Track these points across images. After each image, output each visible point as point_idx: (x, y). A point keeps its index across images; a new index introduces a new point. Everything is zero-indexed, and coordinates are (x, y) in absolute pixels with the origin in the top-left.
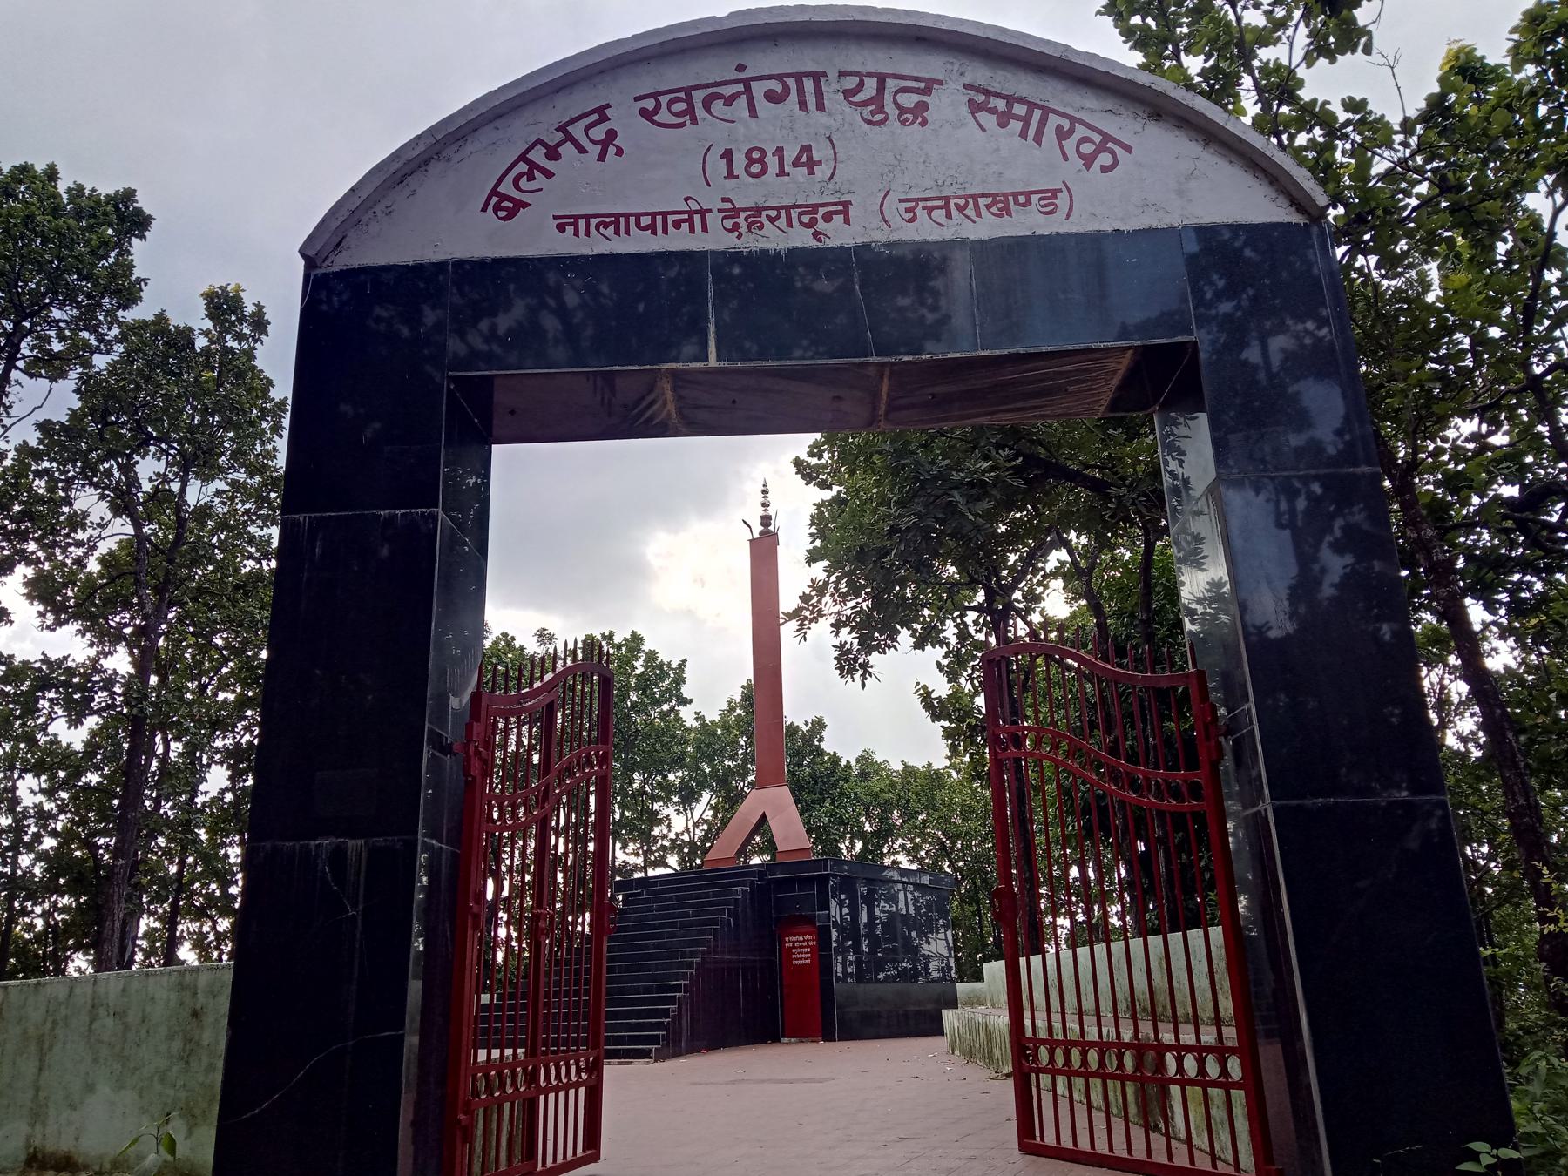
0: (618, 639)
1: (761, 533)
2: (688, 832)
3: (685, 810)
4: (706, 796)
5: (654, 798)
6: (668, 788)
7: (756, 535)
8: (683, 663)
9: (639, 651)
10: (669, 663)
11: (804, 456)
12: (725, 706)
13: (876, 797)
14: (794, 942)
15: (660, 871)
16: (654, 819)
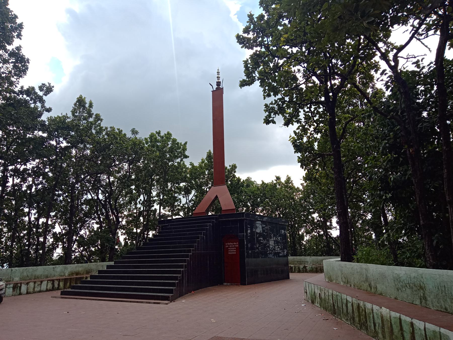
0: (162, 134)
1: (216, 88)
2: (187, 204)
3: (186, 196)
4: (193, 192)
5: (175, 192)
6: (180, 189)
7: (215, 89)
8: (186, 143)
9: (170, 139)
10: (181, 143)
11: (241, 33)
12: (201, 161)
14: (229, 245)
16: (176, 200)
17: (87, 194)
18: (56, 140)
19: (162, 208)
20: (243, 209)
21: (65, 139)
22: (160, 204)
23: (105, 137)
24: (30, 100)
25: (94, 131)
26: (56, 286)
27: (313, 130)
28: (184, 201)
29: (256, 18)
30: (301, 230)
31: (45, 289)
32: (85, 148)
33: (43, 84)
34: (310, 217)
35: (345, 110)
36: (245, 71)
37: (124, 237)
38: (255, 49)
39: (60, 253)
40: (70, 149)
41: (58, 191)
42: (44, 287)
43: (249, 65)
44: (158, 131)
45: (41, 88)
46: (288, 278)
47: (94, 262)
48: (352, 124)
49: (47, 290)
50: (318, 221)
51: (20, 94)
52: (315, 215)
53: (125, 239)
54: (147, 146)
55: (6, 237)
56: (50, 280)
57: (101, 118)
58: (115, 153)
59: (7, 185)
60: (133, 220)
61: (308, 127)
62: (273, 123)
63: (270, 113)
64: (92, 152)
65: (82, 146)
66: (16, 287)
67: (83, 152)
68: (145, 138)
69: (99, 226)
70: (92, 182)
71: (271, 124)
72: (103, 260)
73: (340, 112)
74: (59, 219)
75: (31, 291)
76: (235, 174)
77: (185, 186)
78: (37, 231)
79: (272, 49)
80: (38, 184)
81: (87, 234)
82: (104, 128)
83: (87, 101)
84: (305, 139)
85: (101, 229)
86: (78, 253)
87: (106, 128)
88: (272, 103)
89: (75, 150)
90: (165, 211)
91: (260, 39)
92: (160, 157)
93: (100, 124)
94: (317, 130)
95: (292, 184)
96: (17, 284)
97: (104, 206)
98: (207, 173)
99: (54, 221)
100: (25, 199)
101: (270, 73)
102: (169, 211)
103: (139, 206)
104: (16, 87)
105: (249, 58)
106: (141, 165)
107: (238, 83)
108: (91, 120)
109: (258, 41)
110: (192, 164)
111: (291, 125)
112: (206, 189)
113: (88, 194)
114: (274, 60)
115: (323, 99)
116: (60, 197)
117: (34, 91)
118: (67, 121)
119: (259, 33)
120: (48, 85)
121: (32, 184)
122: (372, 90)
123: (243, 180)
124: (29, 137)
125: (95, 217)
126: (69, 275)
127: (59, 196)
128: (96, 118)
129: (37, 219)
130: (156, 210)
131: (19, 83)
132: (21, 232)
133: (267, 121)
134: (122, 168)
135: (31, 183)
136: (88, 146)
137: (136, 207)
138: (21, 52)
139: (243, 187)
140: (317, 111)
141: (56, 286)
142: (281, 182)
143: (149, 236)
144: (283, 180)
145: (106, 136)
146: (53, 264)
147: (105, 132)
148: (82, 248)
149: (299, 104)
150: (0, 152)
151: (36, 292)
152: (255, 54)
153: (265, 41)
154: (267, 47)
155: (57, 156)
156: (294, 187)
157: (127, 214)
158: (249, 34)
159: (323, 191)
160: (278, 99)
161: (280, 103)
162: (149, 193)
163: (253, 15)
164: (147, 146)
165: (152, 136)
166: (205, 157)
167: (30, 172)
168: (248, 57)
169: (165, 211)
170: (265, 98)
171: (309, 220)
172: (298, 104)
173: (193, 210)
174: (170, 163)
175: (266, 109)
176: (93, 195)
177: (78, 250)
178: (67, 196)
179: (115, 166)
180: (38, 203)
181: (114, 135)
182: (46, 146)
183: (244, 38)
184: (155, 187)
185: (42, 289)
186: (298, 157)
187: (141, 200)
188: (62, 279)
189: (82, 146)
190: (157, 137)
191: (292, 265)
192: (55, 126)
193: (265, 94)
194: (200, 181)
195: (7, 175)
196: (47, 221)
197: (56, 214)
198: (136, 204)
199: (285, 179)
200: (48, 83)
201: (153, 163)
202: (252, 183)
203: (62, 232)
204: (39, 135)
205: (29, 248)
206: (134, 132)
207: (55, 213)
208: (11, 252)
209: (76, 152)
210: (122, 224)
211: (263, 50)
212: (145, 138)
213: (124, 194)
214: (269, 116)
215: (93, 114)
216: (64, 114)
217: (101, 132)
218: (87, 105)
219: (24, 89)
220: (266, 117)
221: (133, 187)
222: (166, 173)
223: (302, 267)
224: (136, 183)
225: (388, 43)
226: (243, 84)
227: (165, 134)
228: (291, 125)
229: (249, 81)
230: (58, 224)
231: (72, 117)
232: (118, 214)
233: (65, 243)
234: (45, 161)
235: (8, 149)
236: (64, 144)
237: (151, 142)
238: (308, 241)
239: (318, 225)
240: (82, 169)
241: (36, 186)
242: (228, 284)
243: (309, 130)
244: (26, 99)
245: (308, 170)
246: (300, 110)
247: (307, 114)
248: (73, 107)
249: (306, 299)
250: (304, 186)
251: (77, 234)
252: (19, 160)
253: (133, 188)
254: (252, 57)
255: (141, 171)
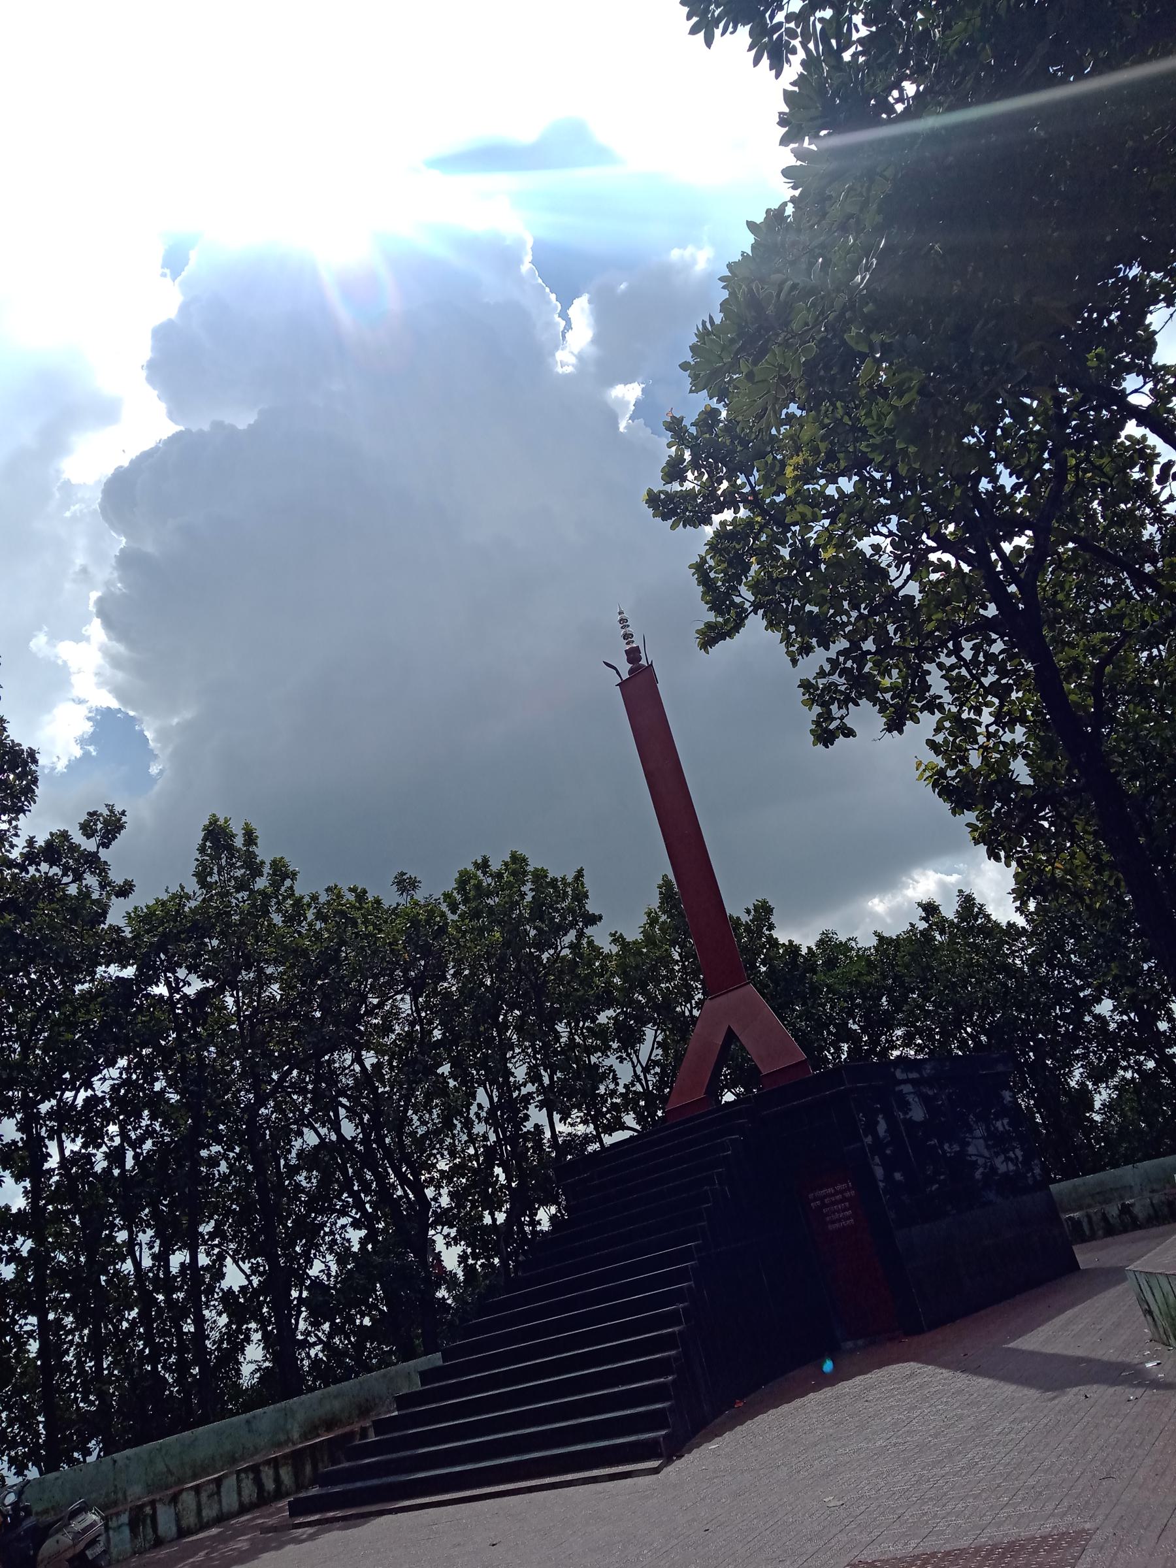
0: (495, 866)
1: (630, 672)
2: (639, 1081)
3: (629, 1055)
4: (649, 1032)
5: (590, 1050)
6: (601, 1033)
7: (625, 676)
8: (580, 874)
9: (525, 873)
10: (563, 879)
11: (658, 485)
12: (644, 919)
13: (855, 983)
14: (822, 1199)
15: (620, 1136)
16: (596, 1075)
17: (300, 1134)
18: (167, 978)
19: (556, 1117)
20: (838, 1050)
21: (191, 969)
22: (549, 1105)
23: (318, 927)
24: (62, 876)
25: (277, 919)
26: (270, 1486)
27: (993, 719)
28: (625, 1073)
29: (692, 425)
30: (1071, 1072)
31: (235, 1506)
32: (263, 980)
33: (90, 814)
34: (1087, 1019)
35: (1087, 618)
36: (704, 594)
37: (458, 1250)
38: (717, 518)
39: (260, 1359)
40: (217, 995)
41: (207, 1146)
42: (230, 1500)
43: (712, 575)
44: (479, 861)
45: (87, 829)
46: (1072, 1266)
47: (378, 1367)
48: (1125, 659)
49: (243, 1509)
50: (1122, 1025)
51: (30, 865)
52: (1105, 1007)
53: (463, 1258)
54: (456, 917)
55: (78, 1345)
56: (245, 1470)
57: (291, 869)
58: (359, 971)
59: (46, 1166)
60: (472, 1184)
61: (972, 716)
62: (846, 736)
63: (825, 705)
64: (286, 987)
65: (252, 975)
66: (140, 1519)
67: (260, 993)
68: (444, 894)
69: (363, 1233)
70: (310, 1087)
71: (841, 740)
72: (407, 1354)
73: (1070, 633)
74: (231, 1241)
75: (192, 1526)
76: (775, 934)
77: (616, 1018)
78: (168, 1299)
79: (773, 501)
80: (141, 1140)
81: (334, 1274)
82: (306, 900)
83: (237, 828)
84: (975, 760)
85: (375, 1243)
86: (319, 1347)
87: (314, 898)
88: (822, 674)
89: (232, 995)
90: (571, 1126)
91: (725, 485)
92: (507, 944)
93: (291, 888)
94: (1005, 719)
95: (988, 917)
96: (143, 1506)
97: (367, 1159)
98: (677, 957)
99: (216, 1251)
100: (111, 1201)
101: (788, 577)
102: (585, 1122)
103: (479, 1128)
104: (12, 846)
105: (707, 552)
106: (454, 989)
107: (694, 641)
108: (261, 883)
109: (719, 492)
110: (617, 939)
111: (909, 723)
112: (691, 1012)
113: (305, 1130)
114: (789, 535)
115: (992, 611)
116: (219, 1165)
117: (68, 841)
118: (187, 909)
119: (717, 467)
120: (106, 812)
121: (121, 1145)
122: (1159, 529)
123: (809, 948)
124: (83, 994)
125: (346, 1205)
126: (305, 1437)
127: (213, 1162)
128: (274, 874)
129: (162, 1258)
130: (538, 1128)
131: (19, 832)
132: (123, 1318)
133: (825, 736)
134: (395, 1013)
135: (117, 1141)
136: (269, 971)
137: (470, 1134)
138: (8, 736)
139: (815, 973)
140: (986, 655)
141: (270, 1486)
142: (944, 920)
143: (538, 1228)
144: (949, 911)
145: (318, 922)
146: (247, 1408)
147: (312, 910)
148: (326, 1326)
149: (916, 650)
150: (8, 1065)
151: (208, 1522)
152: (720, 535)
153: (743, 486)
154: (755, 502)
155: (180, 1029)
156: (997, 925)
157: (447, 1168)
158: (683, 479)
159: (1103, 913)
160: (839, 653)
161: (849, 664)
162: (499, 1076)
163: (682, 419)
164: (456, 917)
165: (464, 880)
166: (655, 902)
167: (108, 1104)
168: (703, 550)
169: (571, 1126)
170: (794, 662)
171: (1089, 1031)
172: (911, 651)
173: (665, 1099)
174: (545, 956)
175: (807, 696)
176: (323, 1131)
177: (316, 1336)
178: (239, 1157)
179: (370, 1012)
180: (154, 1204)
181: (343, 914)
182: (140, 1008)
183: (670, 497)
184: (517, 1050)
185: (225, 1509)
186: (968, 825)
187: (480, 1106)
188: (285, 1456)
189: (252, 975)
190: (480, 882)
191: (1076, 1215)
192: (155, 936)
193: (792, 649)
194: (661, 990)
195: (38, 1134)
196: (194, 1258)
197: (218, 1225)
198: (468, 1124)
199: (956, 907)
200: (107, 805)
201: (490, 971)
202: (844, 947)
203: (250, 1282)
204: (110, 978)
205: (155, 1368)
206: (405, 884)
207: (212, 1223)
208: (103, 1396)
209: (236, 1002)
210: (439, 1207)
211: (743, 513)
212: (444, 894)
213: (420, 1098)
214: (827, 716)
215: (263, 863)
216: (175, 889)
217: (300, 915)
218: (239, 842)
219: (37, 845)
220: (817, 723)
221: (445, 1069)
222: (539, 990)
223: (1113, 1210)
224: (450, 1051)
225: (1157, 368)
226: (711, 637)
227: (506, 864)
228: (909, 723)
229: (726, 621)
230: (233, 1257)
231: (200, 892)
232: (417, 1175)
233: (270, 1323)
234: (147, 1056)
235: (27, 1048)
236: (195, 986)
237: (466, 901)
238: (1109, 1107)
239: (1129, 1041)
240: (267, 1054)
241: (134, 1150)
242: (860, 1342)
243: (980, 724)
244: (50, 874)
245: (1020, 864)
246: (926, 666)
247: (954, 673)
248: (198, 860)
249: (1157, 1338)
250: (1031, 913)
251: (300, 1278)
252: (67, 1075)
253: (446, 1074)
254: (714, 546)
255: (458, 1006)
